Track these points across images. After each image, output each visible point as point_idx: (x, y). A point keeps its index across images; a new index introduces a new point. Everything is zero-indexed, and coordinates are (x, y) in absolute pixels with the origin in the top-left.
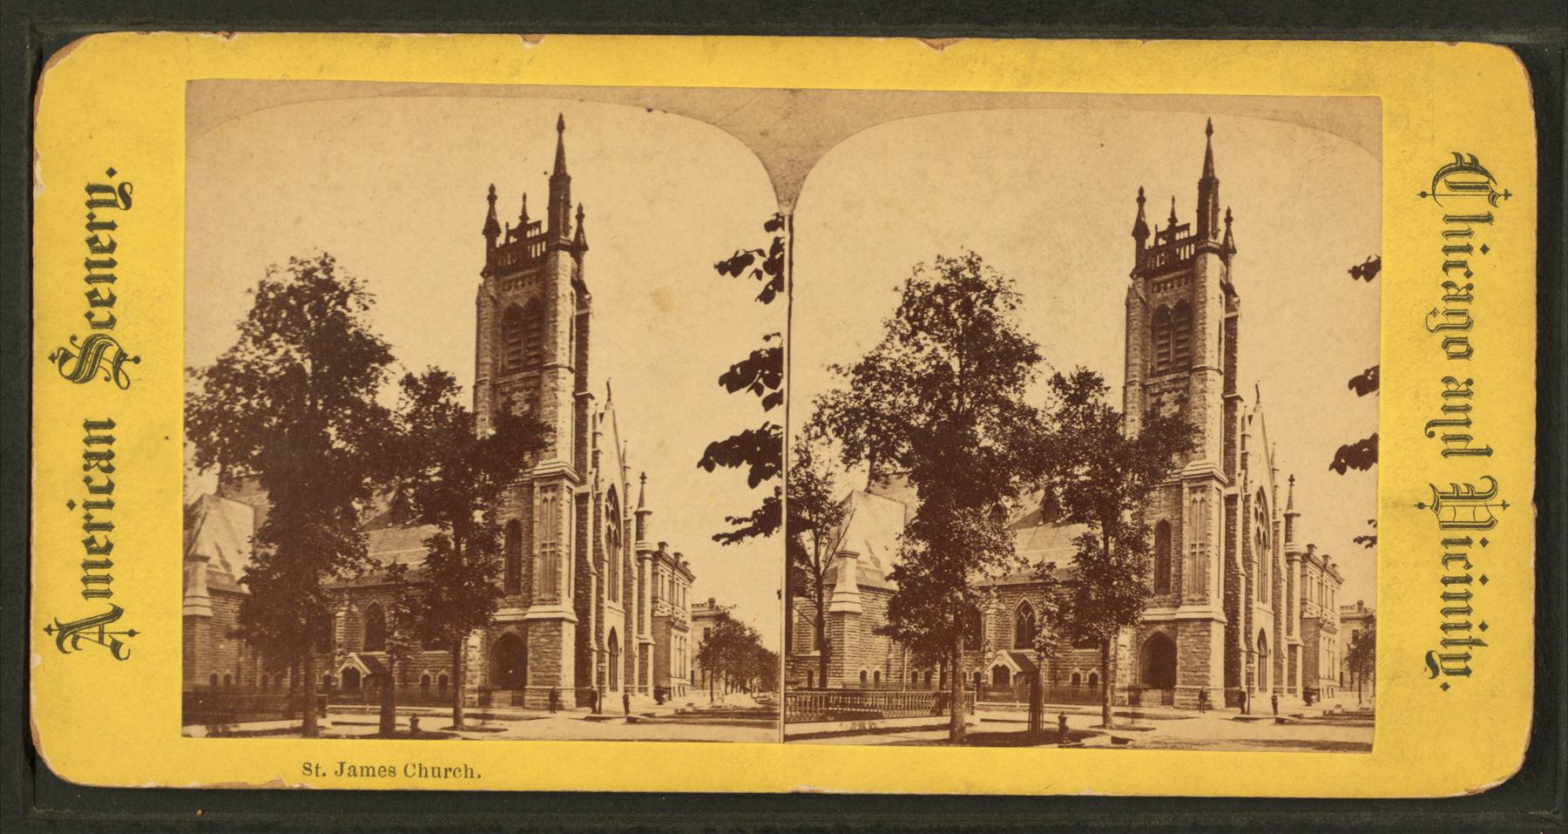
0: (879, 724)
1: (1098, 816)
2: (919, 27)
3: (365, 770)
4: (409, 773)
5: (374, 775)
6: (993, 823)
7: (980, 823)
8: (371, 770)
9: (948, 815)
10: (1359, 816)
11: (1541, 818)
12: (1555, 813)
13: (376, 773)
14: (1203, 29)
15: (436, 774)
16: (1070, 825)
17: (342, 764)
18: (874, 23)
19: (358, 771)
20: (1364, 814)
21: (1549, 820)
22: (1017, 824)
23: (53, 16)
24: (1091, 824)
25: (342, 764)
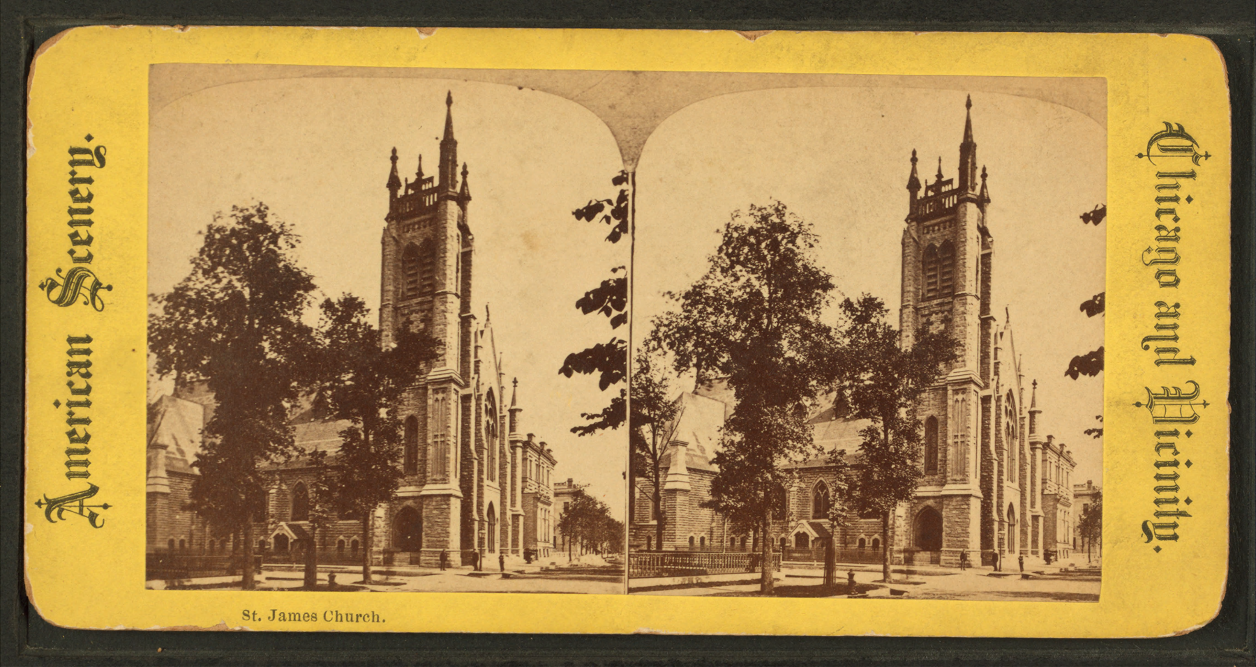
0: (704, 579)
1: (880, 653)
2: (736, 21)
3: (292, 616)
4: (328, 619)
5: (299, 620)
6: (795, 659)
7: (785, 659)
8: (297, 616)
9: (759, 651)
10: (1088, 653)
11: (1235, 654)
12: (1245, 650)
13: (302, 619)
14: (963, 23)
15: (349, 619)
16: (857, 660)
17: (274, 611)
18: (700, 18)
19: (287, 616)
20: (1093, 651)
21: (1241, 656)
22: (815, 659)
23: (42, 13)
24: (874, 659)
25: (274, 611)
